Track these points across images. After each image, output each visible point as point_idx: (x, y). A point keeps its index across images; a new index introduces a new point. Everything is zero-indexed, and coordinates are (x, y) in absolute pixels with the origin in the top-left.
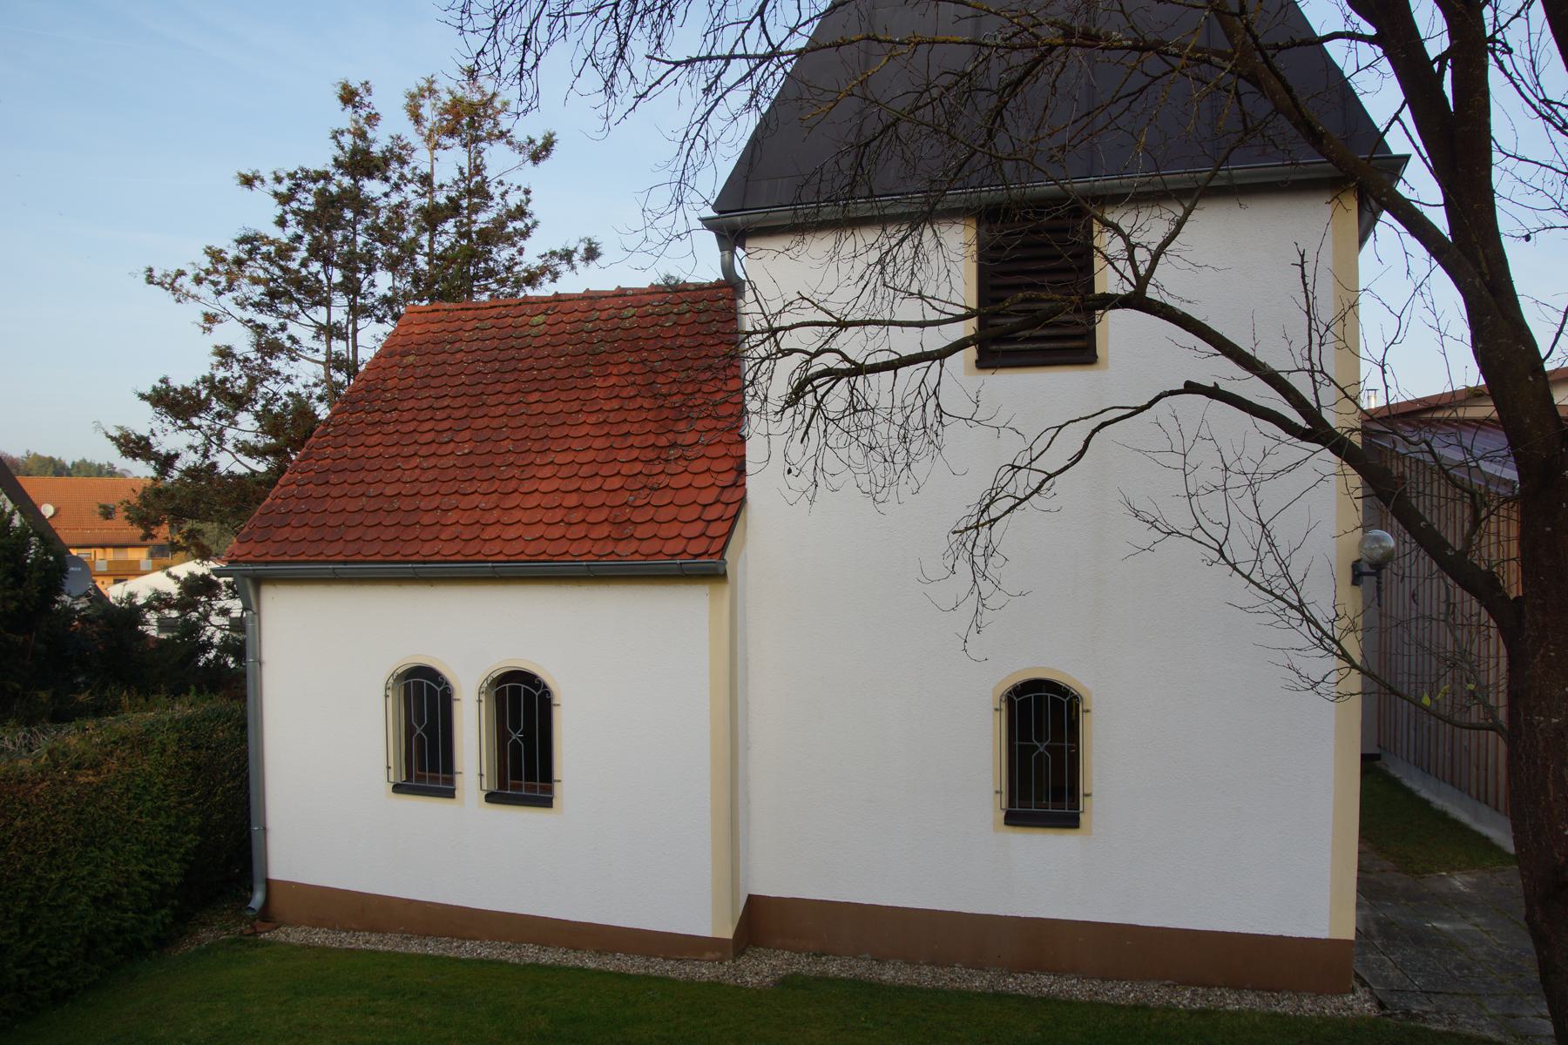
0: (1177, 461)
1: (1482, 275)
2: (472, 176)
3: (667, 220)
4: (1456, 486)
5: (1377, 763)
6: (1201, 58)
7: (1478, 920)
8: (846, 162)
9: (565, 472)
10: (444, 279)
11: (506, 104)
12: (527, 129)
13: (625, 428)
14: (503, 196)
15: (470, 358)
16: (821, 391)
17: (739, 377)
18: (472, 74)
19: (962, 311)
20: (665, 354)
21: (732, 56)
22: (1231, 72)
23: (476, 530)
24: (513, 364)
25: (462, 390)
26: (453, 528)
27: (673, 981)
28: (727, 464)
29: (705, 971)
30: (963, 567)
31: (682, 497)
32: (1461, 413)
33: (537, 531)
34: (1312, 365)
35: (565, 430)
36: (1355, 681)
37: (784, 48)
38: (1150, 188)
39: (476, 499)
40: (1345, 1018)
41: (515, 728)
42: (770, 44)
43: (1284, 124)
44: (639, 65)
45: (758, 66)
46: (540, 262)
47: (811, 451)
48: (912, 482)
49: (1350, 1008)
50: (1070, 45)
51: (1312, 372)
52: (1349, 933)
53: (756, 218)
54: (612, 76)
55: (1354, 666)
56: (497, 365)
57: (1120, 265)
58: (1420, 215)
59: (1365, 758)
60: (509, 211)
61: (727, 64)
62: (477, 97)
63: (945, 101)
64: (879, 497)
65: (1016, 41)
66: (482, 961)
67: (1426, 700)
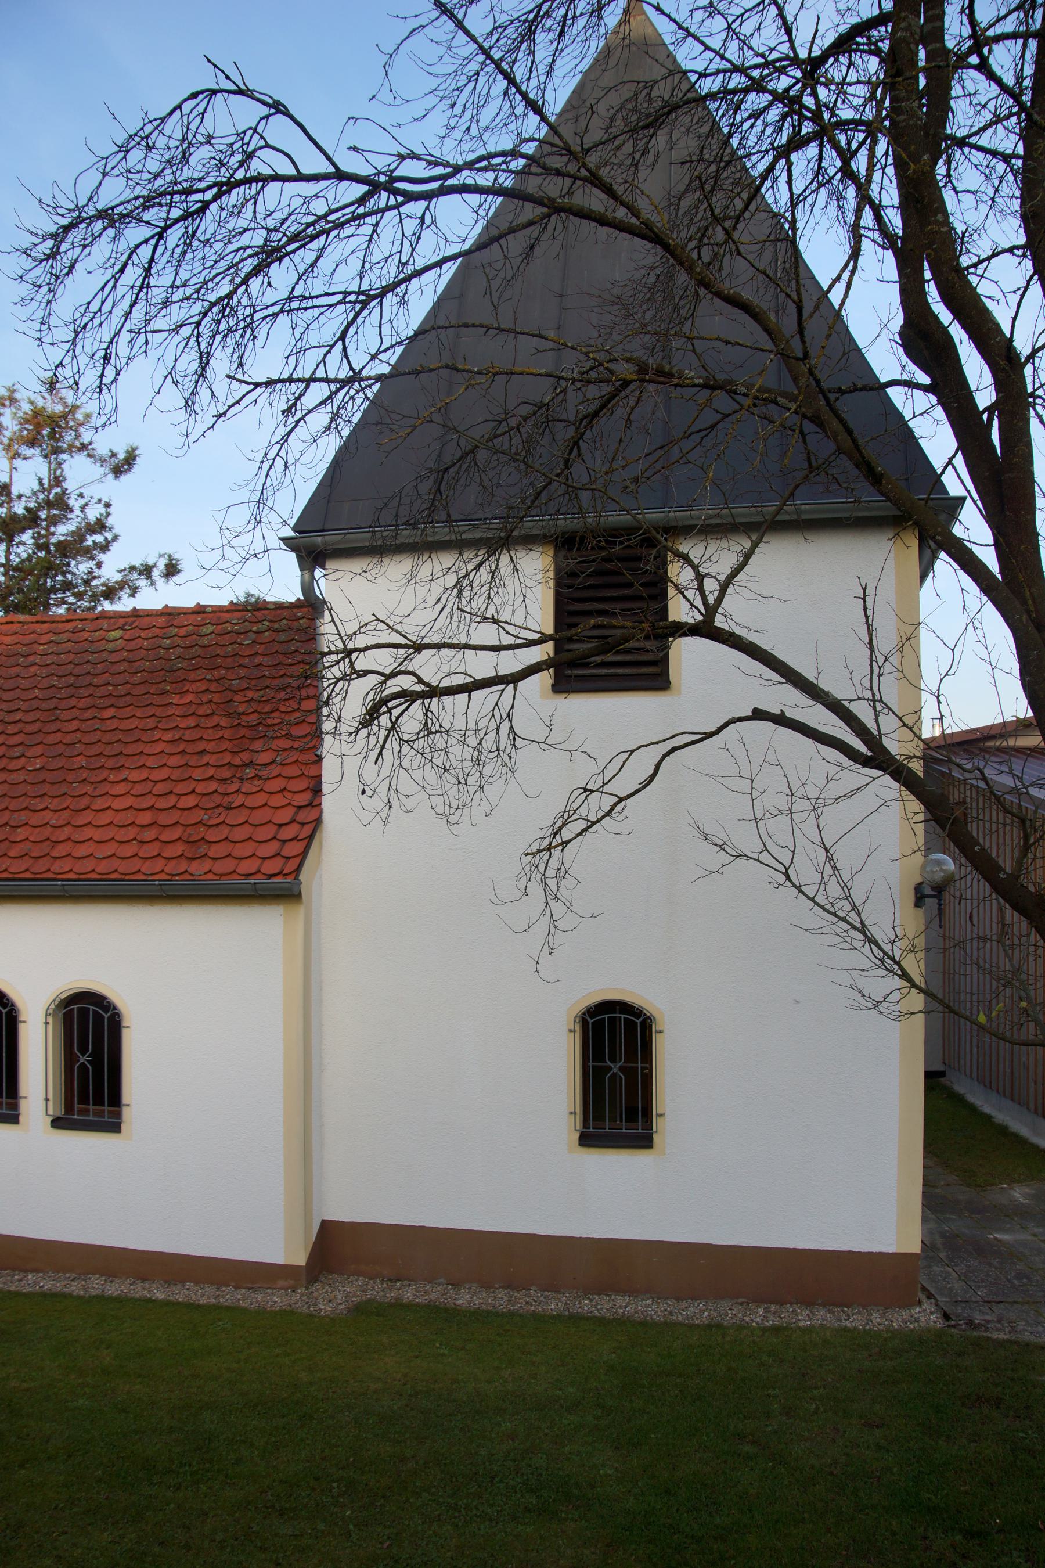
0: (745, 785)
1: (1029, 612)
2: (51, 487)
3: (245, 539)
4: (1006, 811)
5: (942, 1079)
6: (766, 398)
7: (1036, 1230)
8: (426, 487)
9: (139, 789)
10: (20, 591)
11: (88, 416)
12: (105, 442)
13: (201, 746)
14: (83, 508)
15: (44, 672)
16: (396, 712)
17: (317, 697)
18: (52, 385)
19: (536, 636)
20: (242, 672)
21: (313, 379)
22: (796, 412)
23: (45, 848)
24: (88, 679)
25: (35, 704)
26: (22, 845)
27: (244, 1311)
28: (303, 784)
29: (277, 1300)
30: (536, 889)
31: (258, 817)
32: (1011, 742)
33: (108, 850)
34: (873, 695)
35: (140, 747)
36: (917, 1001)
37: (364, 373)
38: (718, 521)
39: (47, 815)
40: (912, 1331)
41: (83, 1051)
42: (351, 368)
43: (844, 462)
44: (221, 386)
45: (338, 390)
46: (118, 577)
47: (385, 772)
48: (484, 803)
49: (917, 1320)
50: (643, 381)
51: (874, 701)
52: (916, 1248)
53: (332, 539)
54: (192, 393)
55: (914, 985)
56: (72, 680)
57: (690, 594)
58: (970, 552)
59: (928, 1075)
60: (88, 524)
61: (307, 387)
62: (59, 408)
63: (523, 430)
64: (452, 819)
65: (593, 375)
66: (44, 1295)
67: (982, 1018)
